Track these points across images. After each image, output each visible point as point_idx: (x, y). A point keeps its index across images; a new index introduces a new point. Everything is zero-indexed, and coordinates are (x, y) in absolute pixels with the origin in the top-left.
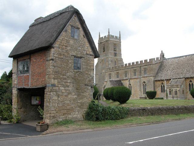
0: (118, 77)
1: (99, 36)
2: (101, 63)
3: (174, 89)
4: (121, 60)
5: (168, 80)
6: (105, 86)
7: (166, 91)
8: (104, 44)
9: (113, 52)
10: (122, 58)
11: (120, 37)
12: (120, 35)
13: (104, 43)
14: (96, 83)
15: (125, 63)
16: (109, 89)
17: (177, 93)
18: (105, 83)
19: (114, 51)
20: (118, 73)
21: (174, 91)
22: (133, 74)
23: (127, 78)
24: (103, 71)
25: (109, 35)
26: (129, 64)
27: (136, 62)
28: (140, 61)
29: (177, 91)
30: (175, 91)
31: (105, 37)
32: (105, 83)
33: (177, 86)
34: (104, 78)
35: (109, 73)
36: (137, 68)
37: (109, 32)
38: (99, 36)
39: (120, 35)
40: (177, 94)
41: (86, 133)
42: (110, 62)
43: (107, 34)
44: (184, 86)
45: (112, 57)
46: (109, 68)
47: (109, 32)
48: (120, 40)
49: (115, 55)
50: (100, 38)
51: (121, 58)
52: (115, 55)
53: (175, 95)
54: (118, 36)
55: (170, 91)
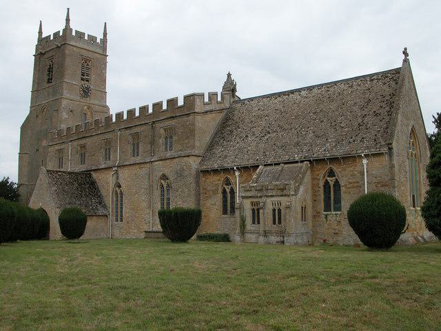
0: (83, 162)
1: (40, 32)
2: (40, 117)
3: (269, 200)
5: (246, 168)
7: (241, 208)
8: (51, 58)
11: (104, 41)
12: (105, 34)
13: (50, 54)
17: (280, 218)
21: (269, 207)
22: (130, 148)
25: (67, 29)
28: (185, 97)
29: (280, 211)
30: (274, 210)
33: (282, 190)
37: (68, 20)
38: (40, 32)
39: (105, 34)
40: (280, 222)
43: (60, 27)
44: (306, 191)
45: (72, 97)
47: (68, 20)
48: (105, 49)
49: (86, 92)
50: (41, 40)
52: (86, 92)
53: (274, 223)
54: (100, 37)
55: (253, 210)
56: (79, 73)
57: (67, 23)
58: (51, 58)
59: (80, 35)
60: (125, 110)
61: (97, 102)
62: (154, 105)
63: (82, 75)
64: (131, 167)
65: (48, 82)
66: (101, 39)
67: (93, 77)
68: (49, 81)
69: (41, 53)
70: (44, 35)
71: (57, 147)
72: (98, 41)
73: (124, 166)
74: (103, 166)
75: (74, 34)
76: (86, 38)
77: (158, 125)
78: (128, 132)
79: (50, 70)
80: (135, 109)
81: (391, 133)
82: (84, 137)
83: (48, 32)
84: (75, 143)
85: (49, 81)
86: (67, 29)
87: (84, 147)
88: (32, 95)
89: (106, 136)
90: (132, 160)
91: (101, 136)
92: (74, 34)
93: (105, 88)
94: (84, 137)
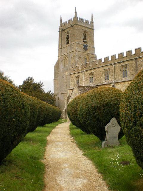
0: (91, 81)
1: (61, 21)
2: (64, 61)
4: (94, 56)
6: (69, 96)
8: (68, 32)
9: (82, 43)
10: (96, 53)
11: (92, 23)
12: (92, 19)
13: (67, 30)
14: (56, 92)
15: (98, 58)
16: (75, 101)
18: (70, 92)
19: (84, 42)
20: (91, 74)
22: (121, 74)
23: (108, 82)
24: (67, 73)
25: (76, 17)
26: (107, 59)
27: (136, 50)
28: (105, 58)
31: (70, 21)
32: (70, 92)
34: (67, 84)
35: (76, 75)
36: (129, 62)
37: (76, 13)
38: (61, 21)
39: (92, 19)
41: (83, 53)
42: (77, 59)
43: (72, 17)
45: (80, 50)
46: (76, 68)
47: (76, 13)
48: (92, 26)
49: (86, 48)
50: (61, 24)
51: (93, 53)
52: (86, 48)
54: (90, 21)
56: (82, 38)
57: (75, 14)
58: (68, 32)
59: (82, 20)
60: (109, 55)
61: (91, 53)
62: (119, 55)
63: (84, 39)
64: (124, 83)
65: (67, 44)
66: (91, 22)
67: (88, 40)
68: (67, 43)
69: (63, 30)
70: (63, 22)
71: (76, 75)
72: (90, 23)
73: (118, 83)
74: (105, 83)
75: (79, 19)
76: (84, 21)
77: (139, 60)
78: (119, 65)
79: (68, 38)
80: (123, 53)
81: (135, 148)
82: (91, 69)
83: (65, 20)
84: (86, 73)
85: (67, 43)
86: (76, 17)
87: (92, 74)
88: (59, 51)
89: (106, 68)
90: (124, 79)
91: (102, 68)
92: (79, 19)
93: (94, 46)
94: (91, 69)
